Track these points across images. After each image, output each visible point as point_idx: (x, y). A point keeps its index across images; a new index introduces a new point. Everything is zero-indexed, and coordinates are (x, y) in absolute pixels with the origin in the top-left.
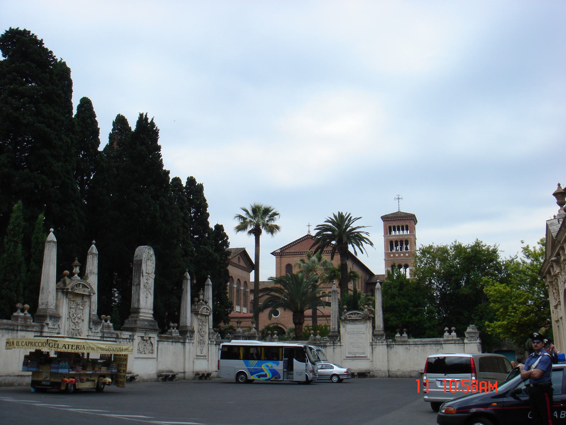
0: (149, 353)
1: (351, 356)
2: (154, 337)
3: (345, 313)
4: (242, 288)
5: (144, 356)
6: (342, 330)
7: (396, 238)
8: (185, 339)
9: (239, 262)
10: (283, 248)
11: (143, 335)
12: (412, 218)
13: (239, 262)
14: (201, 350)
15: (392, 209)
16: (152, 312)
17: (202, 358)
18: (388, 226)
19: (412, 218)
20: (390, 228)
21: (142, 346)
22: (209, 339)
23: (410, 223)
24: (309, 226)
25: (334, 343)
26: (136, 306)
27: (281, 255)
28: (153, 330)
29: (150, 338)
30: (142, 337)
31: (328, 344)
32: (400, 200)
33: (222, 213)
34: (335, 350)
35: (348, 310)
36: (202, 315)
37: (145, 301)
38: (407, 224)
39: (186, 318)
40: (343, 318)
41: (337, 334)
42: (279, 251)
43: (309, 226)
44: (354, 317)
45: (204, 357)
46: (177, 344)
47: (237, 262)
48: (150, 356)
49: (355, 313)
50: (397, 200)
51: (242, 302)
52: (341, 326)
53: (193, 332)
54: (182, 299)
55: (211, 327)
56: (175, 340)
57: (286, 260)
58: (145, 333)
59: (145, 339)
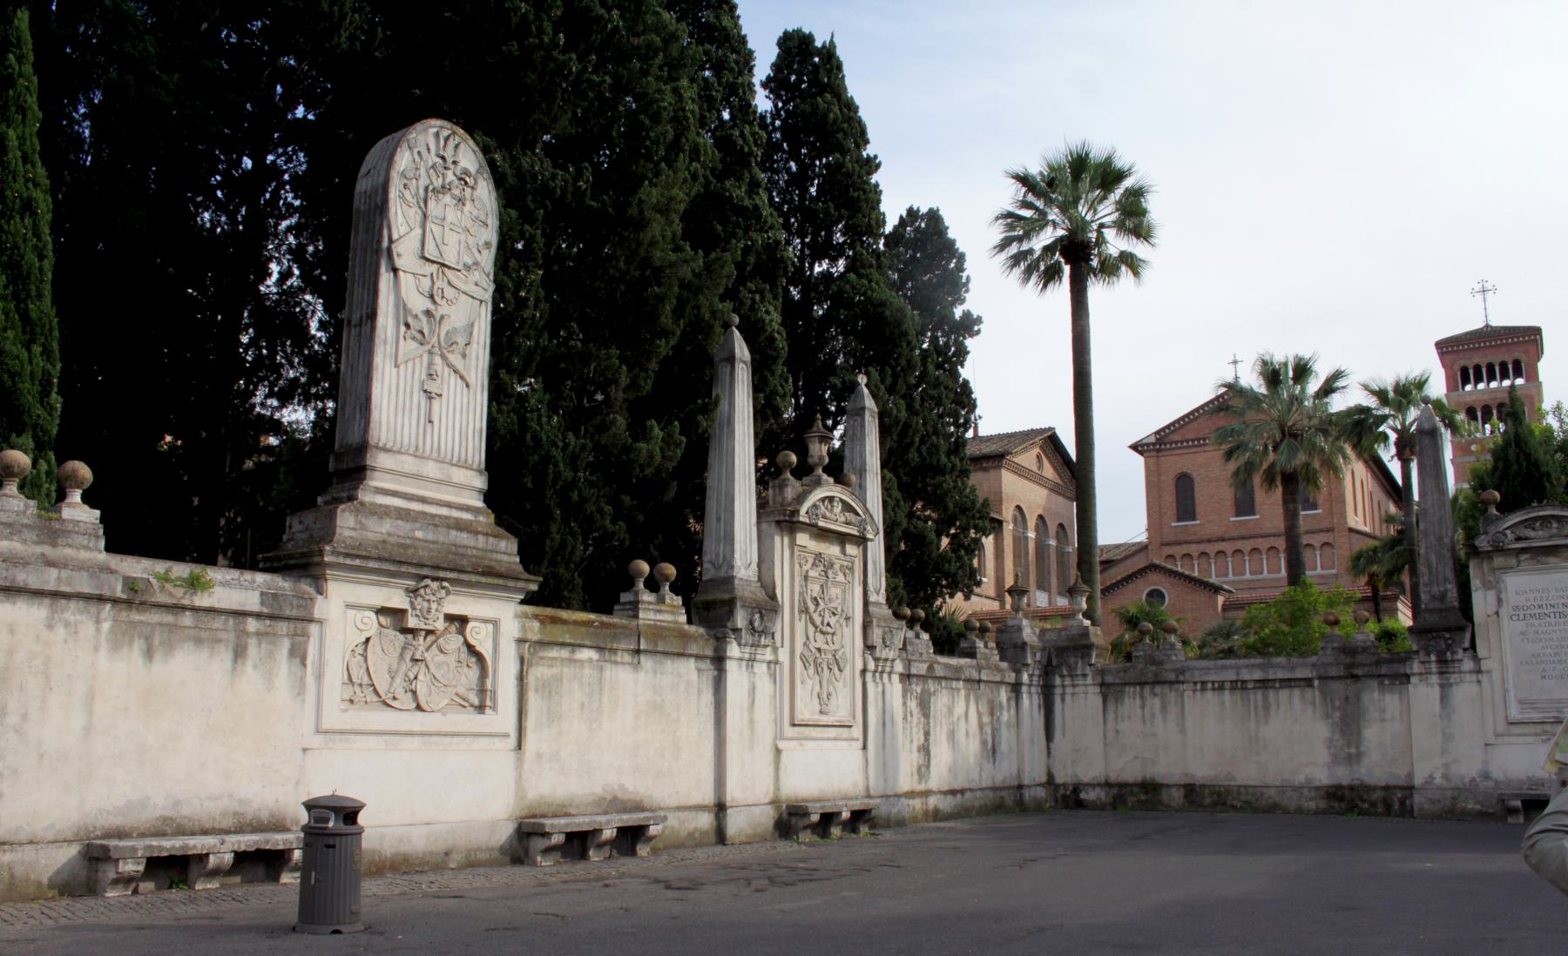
0: (462, 704)
1: (1535, 716)
2: (499, 619)
3: (1491, 521)
4: (1053, 543)
5: (416, 721)
6: (1482, 602)
7: (1486, 399)
8: (720, 642)
9: (1040, 466)
10: (1163, 429)
11: (398, 600)
12: (1529, 339)
13: (1040, 466)
14: (824, 699)
15: (1467, 321)
16: (481, 482)
17: (832, 732)
18: (1457, 367)
19: (1529, 339)
20: (1464, 371)
21: (382, 661)
22: (869, 648)
23: (1526, 352)
24: (1235, 362)
25: (1442, 662)
26: (354, 438)
27: (1158, 451)
28: (487, 576)
29: (462, 621)
30: (397, 614)
31: (1416, 667)
32: (1489, 295)
33: (939, 163)
34: (707, 796)
35: (1506, 507)
36: (823, 534)
37: (428, 412)
38: (1517, 355)
39: (729, 538)
40: (1482, 543)
41: (1455, 618)
42: (1153, 439)
43: (1235, 362)
44: (1539, 538)
45: (844, 732)
46: (670, 665)
47: (1035, 469)
48: (468, 721)
49: (1546, 520)
50: (1479, 297)
51: (1054, 581)
52: (1475, 583)
53: (768, 606)
54: (712, 455)
55: (879, 597)
56: (664, 645)
57: (1175, 464)
58: (413, 592)
59: (412, 622)
